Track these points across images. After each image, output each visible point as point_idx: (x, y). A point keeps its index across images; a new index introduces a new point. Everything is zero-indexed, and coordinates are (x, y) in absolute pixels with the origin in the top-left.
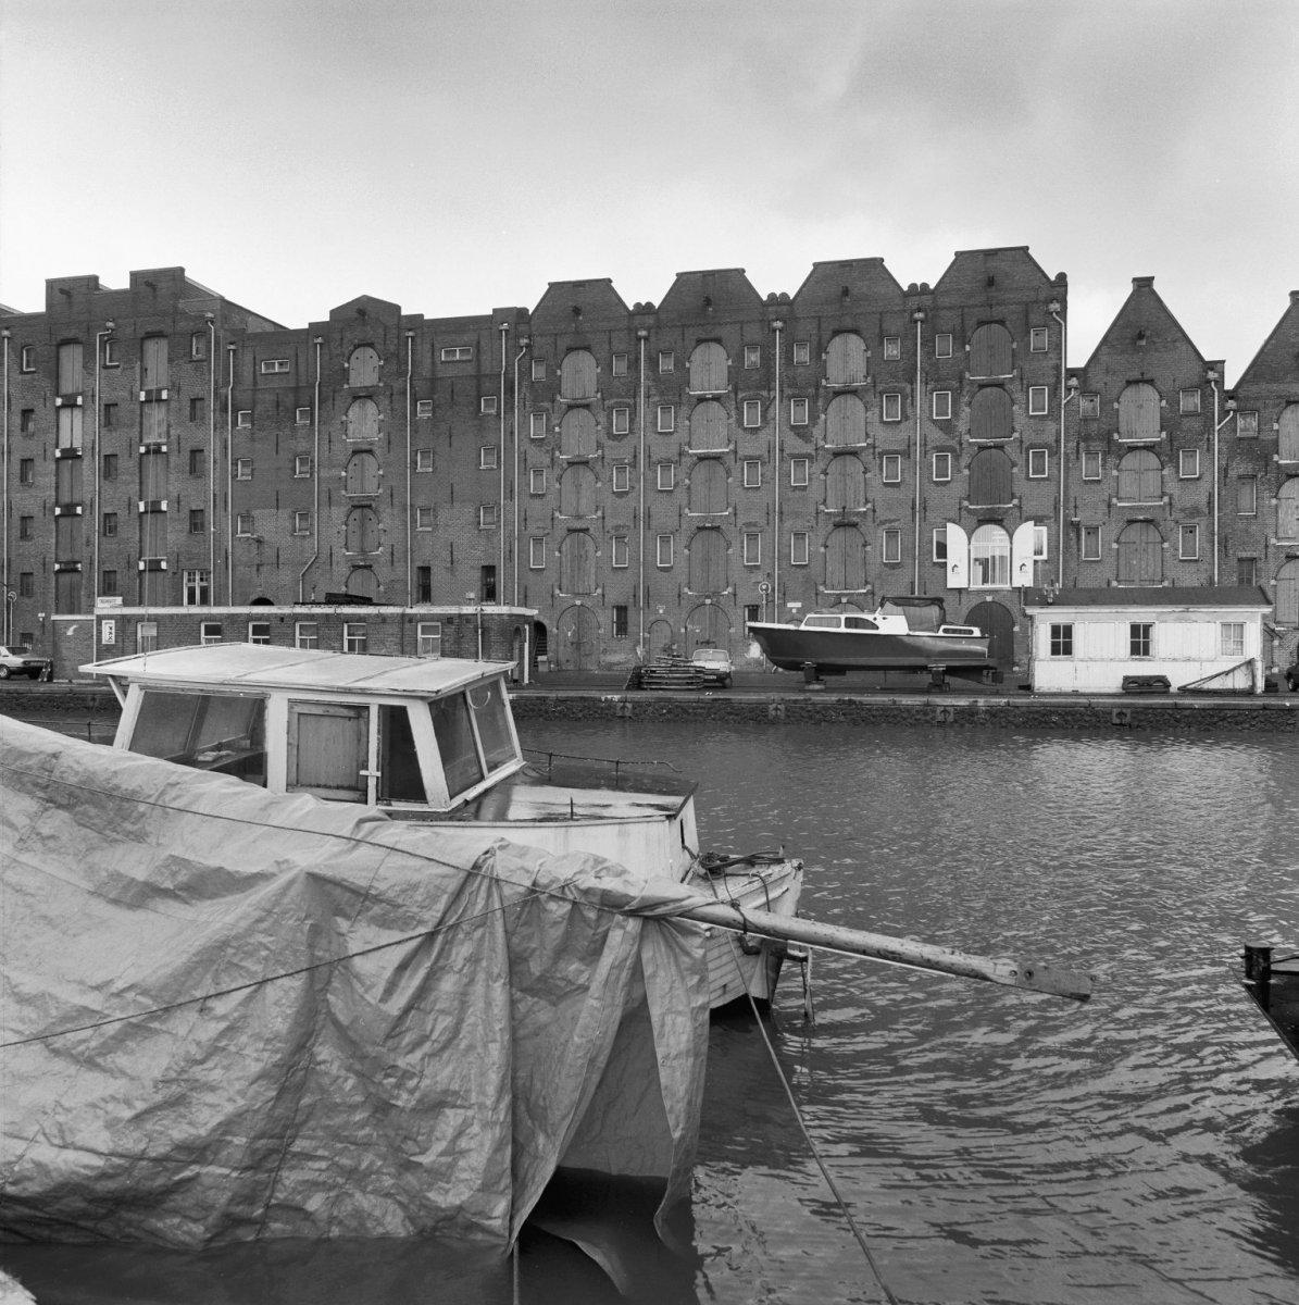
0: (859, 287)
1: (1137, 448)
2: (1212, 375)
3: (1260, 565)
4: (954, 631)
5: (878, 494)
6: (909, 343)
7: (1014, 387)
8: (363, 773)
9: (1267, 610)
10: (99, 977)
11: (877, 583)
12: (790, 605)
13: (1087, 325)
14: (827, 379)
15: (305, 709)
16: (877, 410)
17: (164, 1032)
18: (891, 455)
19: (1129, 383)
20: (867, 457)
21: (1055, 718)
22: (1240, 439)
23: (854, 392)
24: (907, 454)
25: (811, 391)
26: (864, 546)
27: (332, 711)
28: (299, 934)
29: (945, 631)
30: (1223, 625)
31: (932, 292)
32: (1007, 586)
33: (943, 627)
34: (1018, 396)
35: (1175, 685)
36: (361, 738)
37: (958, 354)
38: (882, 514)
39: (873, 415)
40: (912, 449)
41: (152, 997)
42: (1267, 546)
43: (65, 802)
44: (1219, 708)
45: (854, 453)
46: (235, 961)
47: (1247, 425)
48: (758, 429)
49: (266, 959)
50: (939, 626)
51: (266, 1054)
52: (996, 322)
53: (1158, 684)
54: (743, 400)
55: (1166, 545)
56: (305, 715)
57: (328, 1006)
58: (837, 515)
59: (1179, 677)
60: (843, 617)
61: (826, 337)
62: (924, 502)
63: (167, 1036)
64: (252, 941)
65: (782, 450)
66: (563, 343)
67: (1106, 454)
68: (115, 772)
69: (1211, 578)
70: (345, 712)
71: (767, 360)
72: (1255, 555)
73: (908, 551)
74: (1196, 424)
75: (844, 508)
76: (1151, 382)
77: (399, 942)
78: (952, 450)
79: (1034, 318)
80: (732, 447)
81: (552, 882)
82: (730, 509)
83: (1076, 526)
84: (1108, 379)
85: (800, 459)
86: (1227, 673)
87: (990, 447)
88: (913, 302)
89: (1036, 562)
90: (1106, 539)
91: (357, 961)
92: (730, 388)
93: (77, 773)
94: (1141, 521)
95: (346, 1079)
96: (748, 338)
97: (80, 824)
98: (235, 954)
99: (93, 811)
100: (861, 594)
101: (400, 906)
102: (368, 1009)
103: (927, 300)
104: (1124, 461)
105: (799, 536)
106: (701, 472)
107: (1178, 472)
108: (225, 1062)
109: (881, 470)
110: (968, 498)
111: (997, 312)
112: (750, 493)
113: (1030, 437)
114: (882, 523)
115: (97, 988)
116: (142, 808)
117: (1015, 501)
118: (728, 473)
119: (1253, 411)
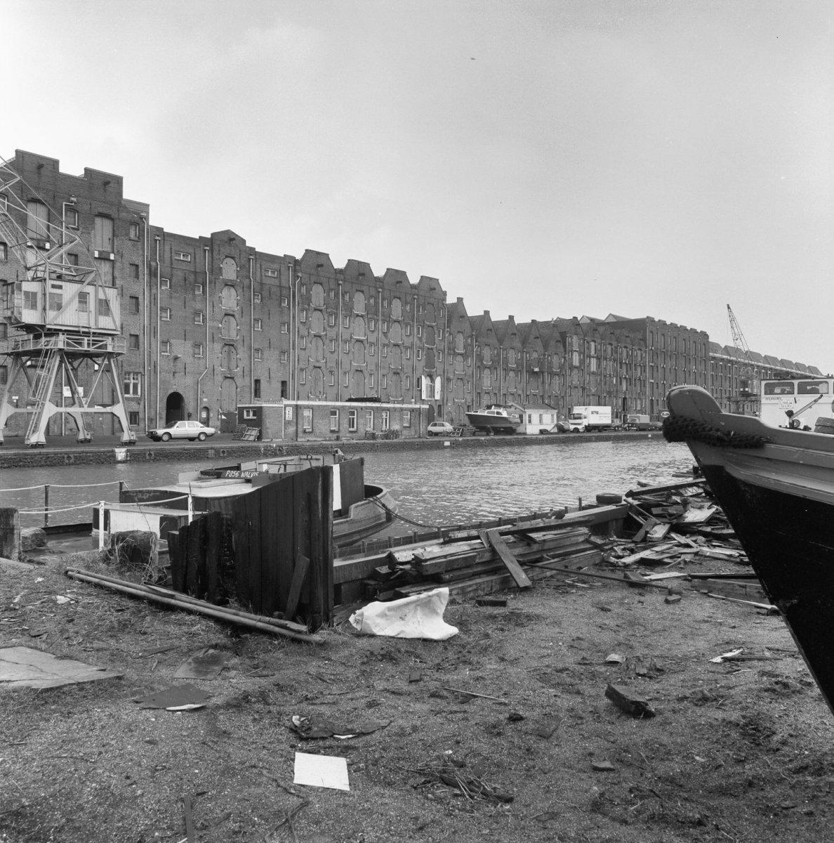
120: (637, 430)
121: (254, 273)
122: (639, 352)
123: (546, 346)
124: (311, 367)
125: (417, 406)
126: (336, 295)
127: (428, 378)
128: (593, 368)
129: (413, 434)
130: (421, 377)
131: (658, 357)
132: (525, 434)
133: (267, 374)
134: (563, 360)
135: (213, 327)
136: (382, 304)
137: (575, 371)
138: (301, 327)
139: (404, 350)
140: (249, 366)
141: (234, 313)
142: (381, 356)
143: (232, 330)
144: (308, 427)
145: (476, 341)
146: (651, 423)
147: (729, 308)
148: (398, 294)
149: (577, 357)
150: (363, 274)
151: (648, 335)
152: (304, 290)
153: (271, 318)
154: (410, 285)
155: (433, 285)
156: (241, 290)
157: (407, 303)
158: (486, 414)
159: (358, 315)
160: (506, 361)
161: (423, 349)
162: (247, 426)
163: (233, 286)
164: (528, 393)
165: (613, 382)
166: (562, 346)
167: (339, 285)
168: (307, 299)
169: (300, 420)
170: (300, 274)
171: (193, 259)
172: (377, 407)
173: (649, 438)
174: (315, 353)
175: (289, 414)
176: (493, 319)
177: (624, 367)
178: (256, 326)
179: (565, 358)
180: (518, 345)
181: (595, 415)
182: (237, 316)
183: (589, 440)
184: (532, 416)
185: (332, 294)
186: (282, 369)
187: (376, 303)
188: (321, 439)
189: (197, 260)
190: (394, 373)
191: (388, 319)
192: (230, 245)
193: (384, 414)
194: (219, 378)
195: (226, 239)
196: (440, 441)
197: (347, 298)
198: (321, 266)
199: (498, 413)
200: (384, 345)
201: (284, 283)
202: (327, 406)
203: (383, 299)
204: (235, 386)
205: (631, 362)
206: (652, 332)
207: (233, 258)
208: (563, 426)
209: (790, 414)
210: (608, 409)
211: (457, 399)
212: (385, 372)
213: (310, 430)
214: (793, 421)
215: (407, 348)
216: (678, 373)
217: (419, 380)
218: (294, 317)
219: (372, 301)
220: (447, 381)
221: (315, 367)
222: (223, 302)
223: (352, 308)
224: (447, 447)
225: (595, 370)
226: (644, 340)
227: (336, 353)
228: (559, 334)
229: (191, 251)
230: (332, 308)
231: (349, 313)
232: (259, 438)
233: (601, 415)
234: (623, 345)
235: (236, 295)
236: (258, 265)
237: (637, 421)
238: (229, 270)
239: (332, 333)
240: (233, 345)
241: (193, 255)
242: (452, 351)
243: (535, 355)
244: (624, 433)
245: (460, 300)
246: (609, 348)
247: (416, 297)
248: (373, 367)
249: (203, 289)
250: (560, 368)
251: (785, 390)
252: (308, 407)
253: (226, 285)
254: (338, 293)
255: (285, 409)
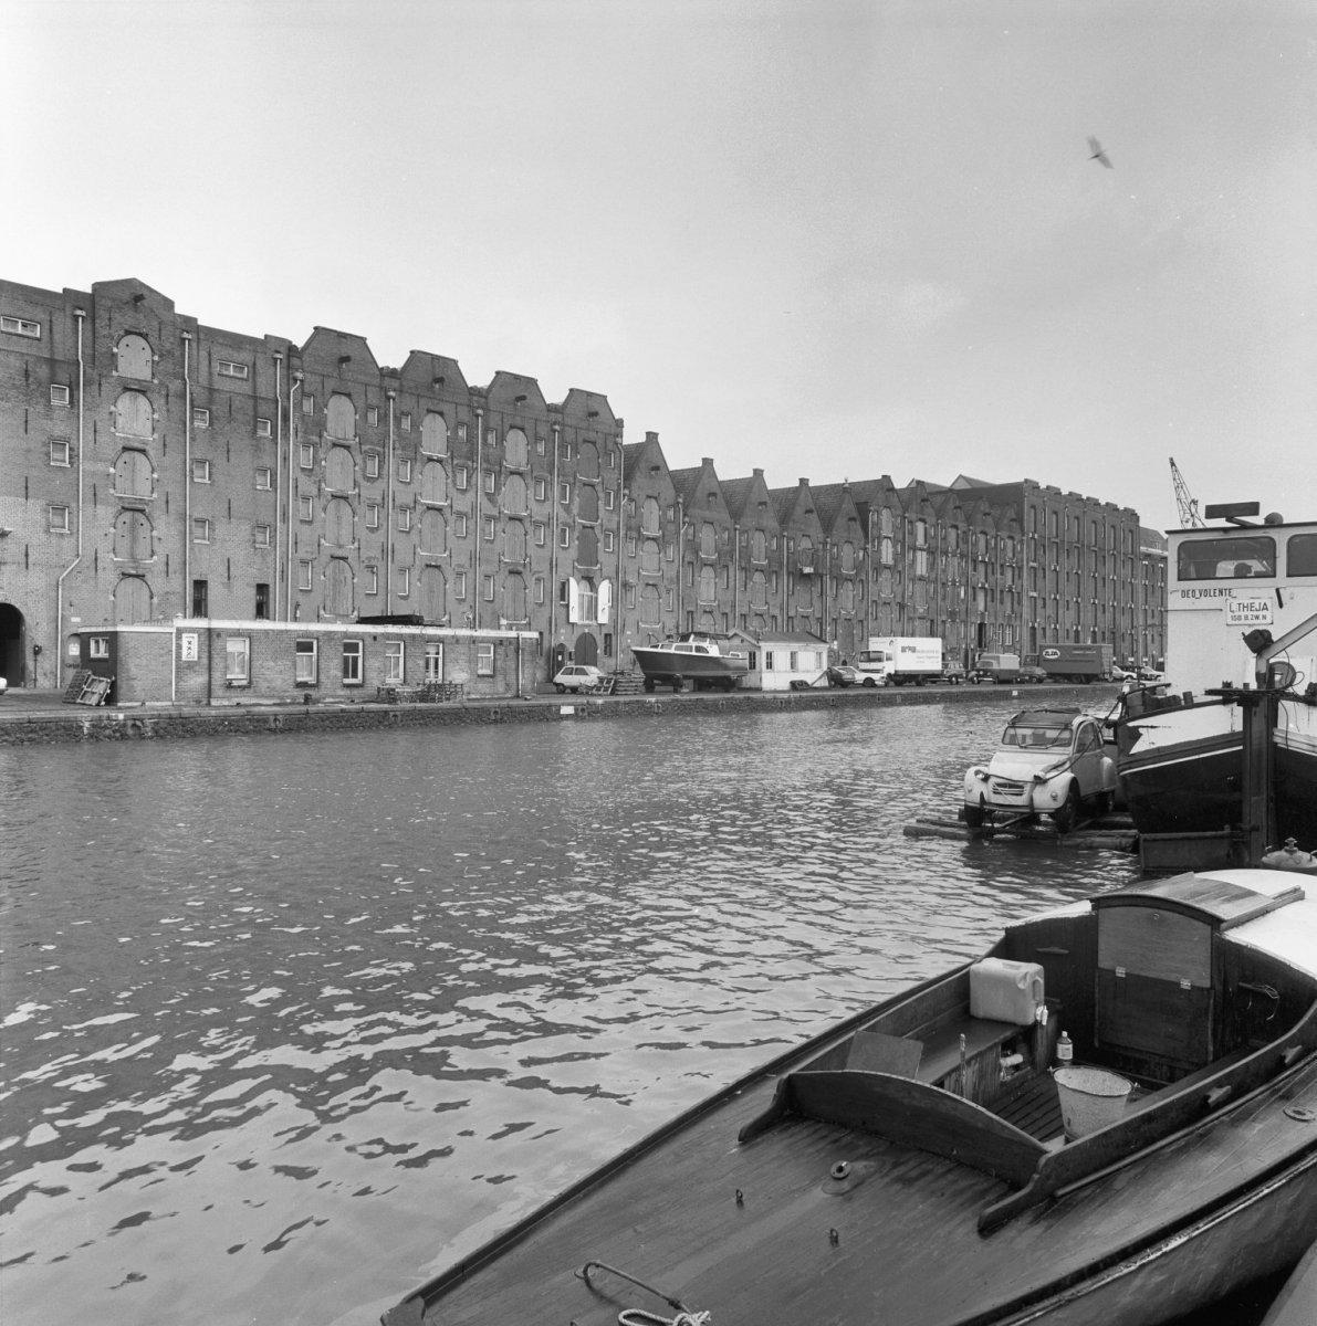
120: (994, 683)
121: (194, 370)
122: (1010, 543)
123: (827, 526)
124: (325, 558)
125: (513, 634)
126: (383, 418)
127: (585, 584)
128: (921, 568)
129: (501, 690)
130: (568, 580)
131: (1044, 552)
132: (759, 690)
133: (222, 569)
134: (861, 554)
135: (94, 474)
136: (485, 440)
137: (886, 574)
138: (302, 478)
139: (530, 529)
140: (181, 552)
141: (147, 448)
142: (482, 540)
143: (141, 480)
144: (238, 675)
145: (685, 515)
146: (1022, 670)
147: (1173, 464)
148: (518, 421)
149: (890, 550)
150: (440, 380)
151: (1028, 516)
152: (308, 406)
153: (232, 459)
155: (596, 407)
156: (163, 401)
157: (538, 439)
158: (672, 651)
159: (430, 459)
160: (747, 552)
161: (572, 528)
162: (94, 674)
163: (143, 392)
164: (792, 613)
165: (959, 594)
166: (859, 527)
167: (388, 398)
168: (319, 425)
169: (217, 660)
170: (299, 375)
171: (46, 333)
172: (413, 636)
173: (1014, 698)
174: (336, 529)
175: (191, 649)
176: (770, 486)
177: (981, 568)
178: (197, 472)
179: (865, 549)
180: (771, 523)
181: (909, 653)
182: (151, 453)
183: (889, 702)
184: (775, 655)
185: (373, 417)
186: (258, 560)
187: (471, 438)
188: (272, 702)
189: (57, 337)
190: (511, 572)
191: (496, 468)
192: (136, 309)
193: (432, 650)
194: (109, 576)
195: (126, 296)
196: (550, 706)
197: (406, 424)
198: (345, 359)
199: (698, 649)
200: (489, 518)
201: (263, 391)
202: (287, 631)
203: (486, 430)
204: (148, 593)
205: (993, 560)
206: (1033, 507)
207: (144, 336)
208: (840, 675)
209: (1259, 642)
210: (936, 644)
211: (646, 623)
212: (489, 569)
213: (245, 683)
214: (1271, 669)
215: (537, 525)
216: (1082, 581)
217: (564, 588)
218: (285, 459)
219: (462, 433)
220: (622, 588)
221: (333, 557)
222: (119, 426)
223: (417, 446)
224: (567, 717)
225: (924, 573)
226: (1019, 520)
227: (382, 531)
228: (856, 507)
229: (43, 316)
230: (372, 443)
231: (411, 450)
232: (111, 699)
233: (922, 654)
234: (949, 522)
235: (149, 409)
236: (203, 354)
237: (995, 667)
238: (135, 360)
239: (372, 492)
240: (142, 511)
241: (47, 327)
242: (635, 532)
243: (806, 544)
244: (966, 688)
245: (652, 436)
246: (953, 533)
247: (557, 427)
248: (464, 560)
249: (71, 396)
250: (855, 567)
251: (1249, 568)
252: (238, 634)
253: (127, 389)
254: (386, 415)
255: (179, 637)
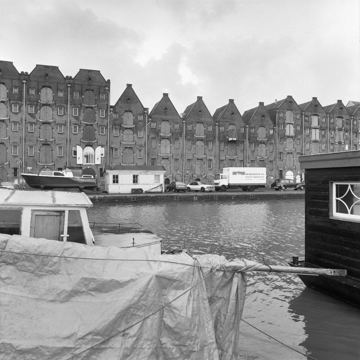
0: (51, 74)
1: (128, 128)
2: (146, 112)
3: (157, 160)
4: (86, 177)
5: (56, 136)
6: (66, 93)
7: (96, 109)
8: (62, 236)
9: (165, 172)
10: (66, 332)
11: (56, 162)
12: (28, 168)
13: (115, 96)
14: (40, 100)
15: (38, 213)
16: (56, 111)
17: (108, 348)
18: (61, 125)
19: (126, 111)
20: (53, 125)
21: (117, 200)
22: (152, 128)
23: (49, 105)
24: (65, 125)
25: (35, 103)
26: (52, 151)
27: (50, 213)
28: (156, 298)
29: (84, 176)
30: (155, 175)
31: (29, 76)
32: (94, 164)
33: (83, 175)
34: (97, 111)
35: (144, 190)
36: (61, 223)
37: (80, 98)
38: (57, 142)
39: (55, 112)
40: (67, 123)
41: (101, 335)
42: (158, 155)
43: (11, 262)
44: (157, 197)
45: (49, 123)
46: (134, 313)
47: (154, 125)
48: (17, 113)
49: (145, 310)
50: (82, 175)
51: (152, 345)
52: (91, 90)
53: (140, 191)
54: (12, 103)
55: (135, 154)
56: (37, 216)
57: (164, 322)
58: (44, 141)
59: (145, 189)
60: (53, 172)
61: (40, 87)
62: (70, 139)
63: (110, 349)
64: (140, 304)
65: (25, 120)
66: (41, 85)
67: (120, 129)
68: (38, 246)
69: (145, 163)
70: (56, 214)
71: (21, 92)
72: (155, 158)
73: (65, 153)
74: (142, 124)
75: (46, 139)
76: (131, 112)
77: (184, 294)
78: (79, 125)
79: (102, 91)
80: (8, 118)
81: (217, 266)
82: (8, 138)
83: (112, 148)
84: (120, 109)
85: (31, 124)
86: (156, 187)
87: (89, 125)
88: (67, 81)
89: (101, 157)
90: (119, 152)
91: (173, 303)
92: (8, 99)
93: (19, 248)
94: (129, 148)
95: (173, 348)
96: (14, 84)
97: (20, 271)
98: (134, 311)
99: (27, 264)
100: (51, 165)
101: (182, 282)
102: (183, 318)
103: (71, 81)
104: (124, 132)
105: (31, 147)
106: (43, 127)
107: (137, 136)
108: (137, 353)
109: (57, 129)
110: (83, 139)
111: (92, 88)
112: (15, 133)
113: (100, 123)
114: (58, 144)
115: (68, 338)
116: (55, 260)
117: (96, 140)
118: (7, 126)
119: (155, 122)
154: (298, 106)
164: (222, 158)
241: (301, 126)
